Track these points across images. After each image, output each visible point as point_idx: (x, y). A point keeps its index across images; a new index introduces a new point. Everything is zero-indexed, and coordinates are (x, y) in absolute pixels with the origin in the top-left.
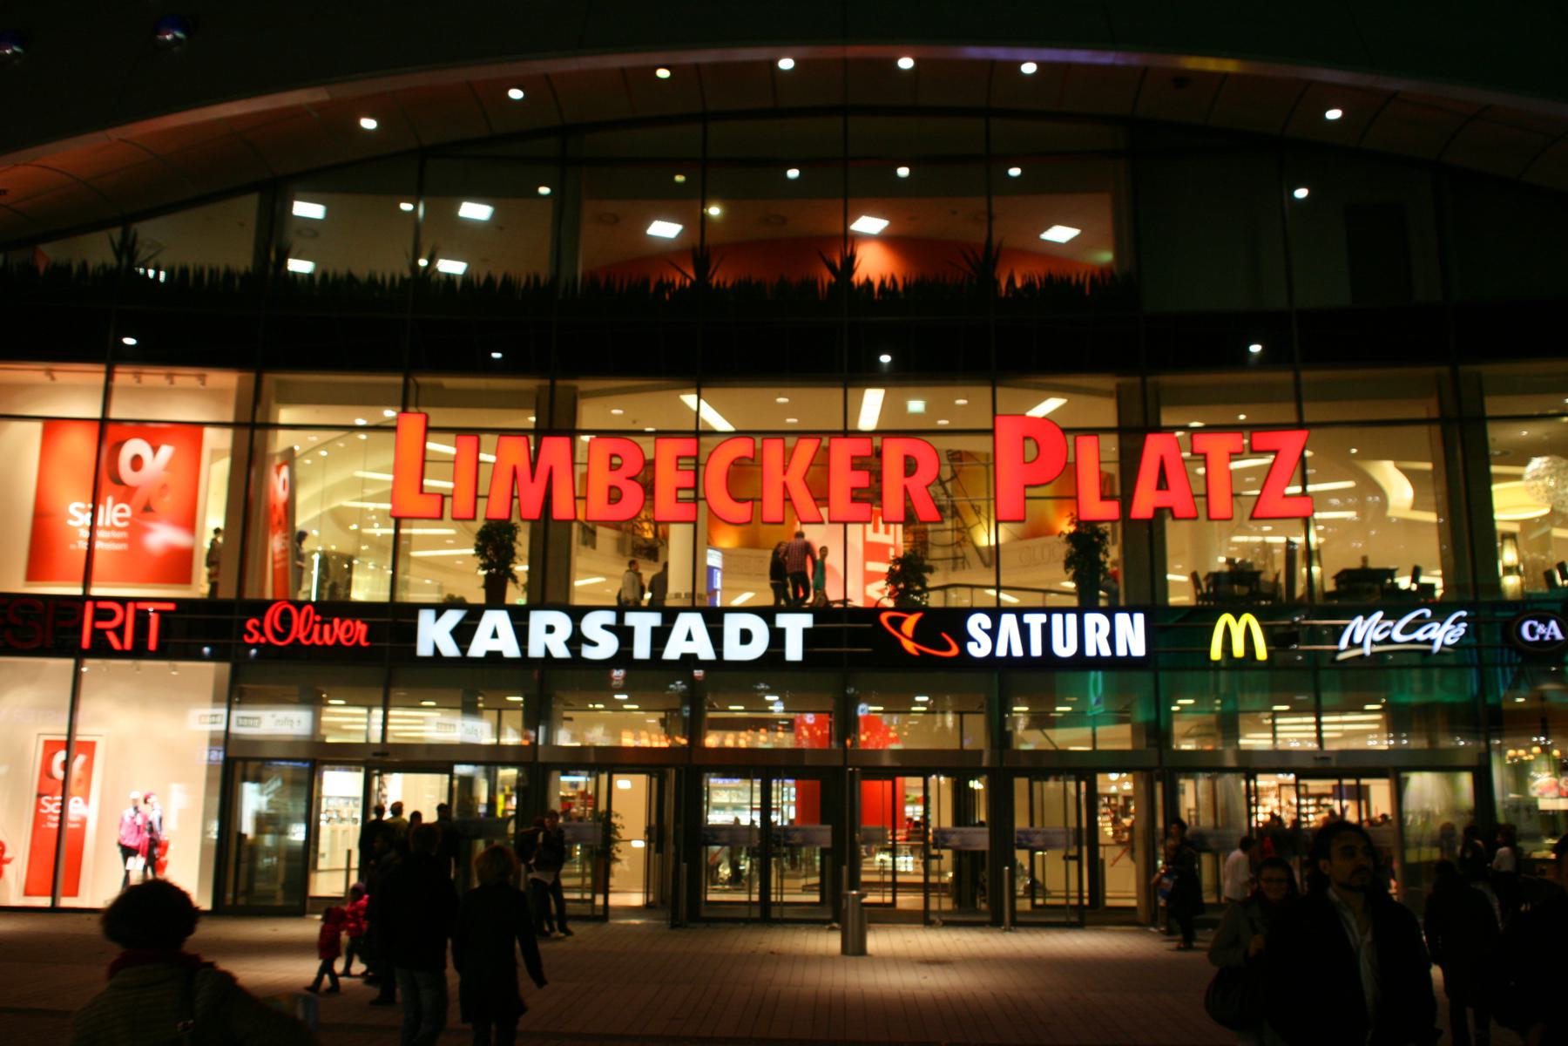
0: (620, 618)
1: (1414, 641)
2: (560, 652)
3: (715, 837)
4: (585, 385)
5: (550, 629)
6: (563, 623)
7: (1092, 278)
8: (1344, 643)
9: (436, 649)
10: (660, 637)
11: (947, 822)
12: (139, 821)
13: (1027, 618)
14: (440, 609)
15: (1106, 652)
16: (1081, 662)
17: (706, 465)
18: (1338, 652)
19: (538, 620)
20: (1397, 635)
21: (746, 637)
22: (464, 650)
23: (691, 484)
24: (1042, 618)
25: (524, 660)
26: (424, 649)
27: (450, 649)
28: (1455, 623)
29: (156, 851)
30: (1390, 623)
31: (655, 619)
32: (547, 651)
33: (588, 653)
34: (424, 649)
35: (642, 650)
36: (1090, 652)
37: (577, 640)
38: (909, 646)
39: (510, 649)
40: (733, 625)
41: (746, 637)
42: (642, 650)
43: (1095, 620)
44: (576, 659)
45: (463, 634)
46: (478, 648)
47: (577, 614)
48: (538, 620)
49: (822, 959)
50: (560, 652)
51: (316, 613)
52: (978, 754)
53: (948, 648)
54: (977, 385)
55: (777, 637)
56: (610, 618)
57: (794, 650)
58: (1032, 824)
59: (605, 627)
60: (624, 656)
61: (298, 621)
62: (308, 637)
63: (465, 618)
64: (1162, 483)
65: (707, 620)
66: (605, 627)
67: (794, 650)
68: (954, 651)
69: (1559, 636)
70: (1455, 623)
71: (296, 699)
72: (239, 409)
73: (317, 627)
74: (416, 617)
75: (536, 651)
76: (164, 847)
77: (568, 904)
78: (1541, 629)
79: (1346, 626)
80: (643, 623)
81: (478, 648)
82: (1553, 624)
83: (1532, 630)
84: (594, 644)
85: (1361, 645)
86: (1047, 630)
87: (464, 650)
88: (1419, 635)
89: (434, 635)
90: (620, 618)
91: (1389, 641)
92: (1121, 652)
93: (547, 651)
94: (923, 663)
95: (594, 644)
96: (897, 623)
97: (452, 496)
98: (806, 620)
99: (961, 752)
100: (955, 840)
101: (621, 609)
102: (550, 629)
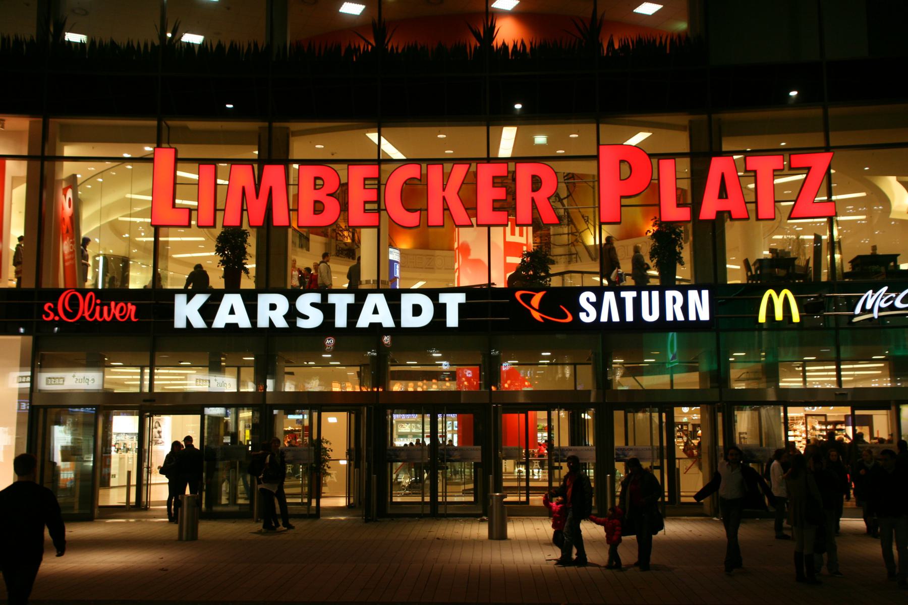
0: (324, 298)
2: (281, 323)
5: (273, 307)
6: (282, 303)
10: (354, 311)
16: (662, 325)
17: (386, 185)
19: (264, 300)
21: (417, 310)
26: (179, 323)
27: (198, 322)
33: (301, 323)
35: (341, 321)
37: (293, 314)
40: (407, 301)
41: (417, 310)
42: (341, 321)
45: (208, 312)
46: (221, 320)
47: (292, 296)
48: (264, 300)
49: (475, 543)
50: (281, 323)
52: (588, 392)
53: (566, 317)
55: (440, 310)
57: (452, 320)
58: (627, 444)
61: (83, 304)
64: (723, 193)
67: (452, 320)
71: (84, 362)
73: (98, 308)
75: (263, 323)
81: (221, 320)
84: (306, 317)
85: (871, 311)
86: (637, 302)
90: (324, 298)
93: (271, 322)
94: (546, 328)
95: (306, 317)
96: (528, 299)
98: (461, 298)
102: (273, 307)
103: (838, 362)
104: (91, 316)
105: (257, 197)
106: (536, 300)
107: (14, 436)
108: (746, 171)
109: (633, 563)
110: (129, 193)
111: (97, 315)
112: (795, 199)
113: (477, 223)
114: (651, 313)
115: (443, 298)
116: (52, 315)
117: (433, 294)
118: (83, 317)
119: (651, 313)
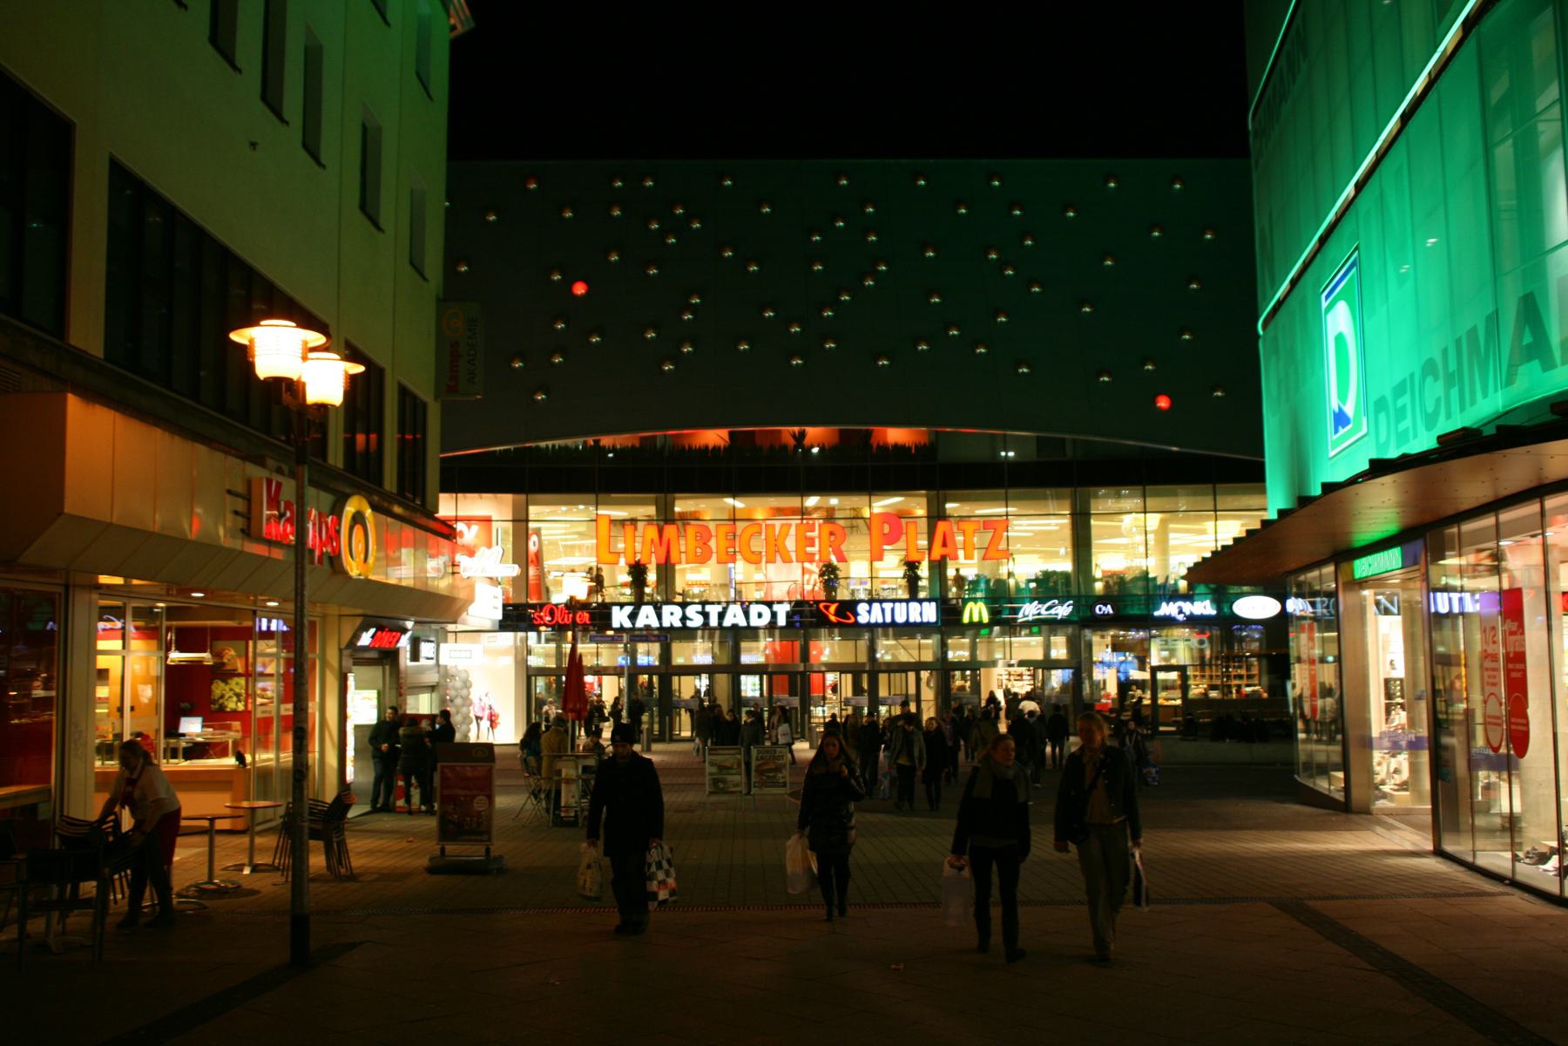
0: (703, 608)
1: (1050, 614)
2: (678, 624)
3: (748, 704)
4: (677, 495)
6: (678, 610)
7: (916, 445)
8: (1020, 615)
9: (621, 625)
10: (721, 616)
11: (850, 694)
12: (482, 704)
13: (885, 605)
14: (622, 605)
15: (919, 620)
16: (1450, 615)
17: (740, 536)
18: (1016, 619)
19: (666, 609)
20: (1043, 611)
21: (760, 615)
22: (634, 624)
23: (905, 547)
24: (891, 605)
25: (661, 628)
27: (628, 624)
28: (1068, 606)
29: (493, 718)
30: (1040, 606)
31: (719, 608)
32: (621, 625)
33: (689, 624)
34: (616, 624)
35: (714, 622)
36: (911, 620)
37: (684, 618)
38: (833, 618)
39: (655, 623)
40: (754, 609)
41: (760, 615)
42: (714, 622)
43: (914, 606)
44: (685, 627)
45: (633, 617)
46: (640, 623)
47: (684, 605)
48: (666, 609)
49: (803, 750)
50: (678, 624)
51: (567, 609)
52: (864, 664)
53: (849, 618)
54: (793, 496)
55: (774, 615)
56: (699, 608)
57: (782, 621)
58: (890, 694)
59: (698, 612)
60: (706, 624)
61: (558, 614)
62: (563, 620)
63: (634, 609)
64: (944, 545)
65: (655, 608)
66: (698, 612)
68: (852, 620)
69: (1111, 612)
70: (1068, 606)
72: (1207, 518)
73: (566, 615)
74: (611, 609)
75: (666, 624)
76: (497, 716)
77: (1161, 709)
78: (1104, 608)
79: (1020, 608)
80: (714, 611)
81: (640, 623)
82: (1109, 606)
83: (1100, 609)
85: (1027, 616)
86: (1461, 600)
87: (634, 624)
88: (1053, 611)
89: (620, 617)
90: (703, 608)
91: (1039, 614)
92: (925, 620)
94: (838, 625)
96: (827, 608)
97: (624, 553)
98: (787, 607)
99: (856, 664)
100: (853, 702)
101: (704, 603)
103: (856, 640)
104: (563, 620)
105: (661, 545)
106: (833, 608)
107: (1344, 832)
108: (958, 529)
109: (154, 643)
110: (740, 509)
111: (566, 620)
112: (986, 546)
113: (797, 558)
114: (1443, 606)
115: (776, 607)
116: (539, 619)
117: (769, 604)
118: (557, 622)
119: (1443, 606)
